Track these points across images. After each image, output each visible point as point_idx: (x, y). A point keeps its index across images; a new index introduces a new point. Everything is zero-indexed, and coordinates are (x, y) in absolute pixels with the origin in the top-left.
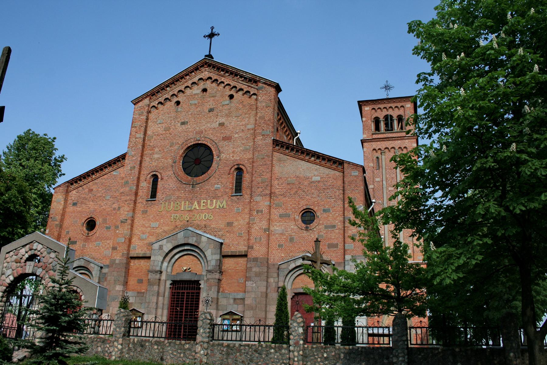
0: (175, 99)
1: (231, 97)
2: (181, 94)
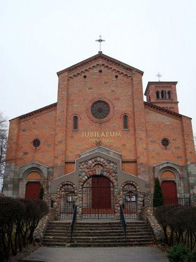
0: (83, 75)
1: (117, 77)
2: (86, 72)
